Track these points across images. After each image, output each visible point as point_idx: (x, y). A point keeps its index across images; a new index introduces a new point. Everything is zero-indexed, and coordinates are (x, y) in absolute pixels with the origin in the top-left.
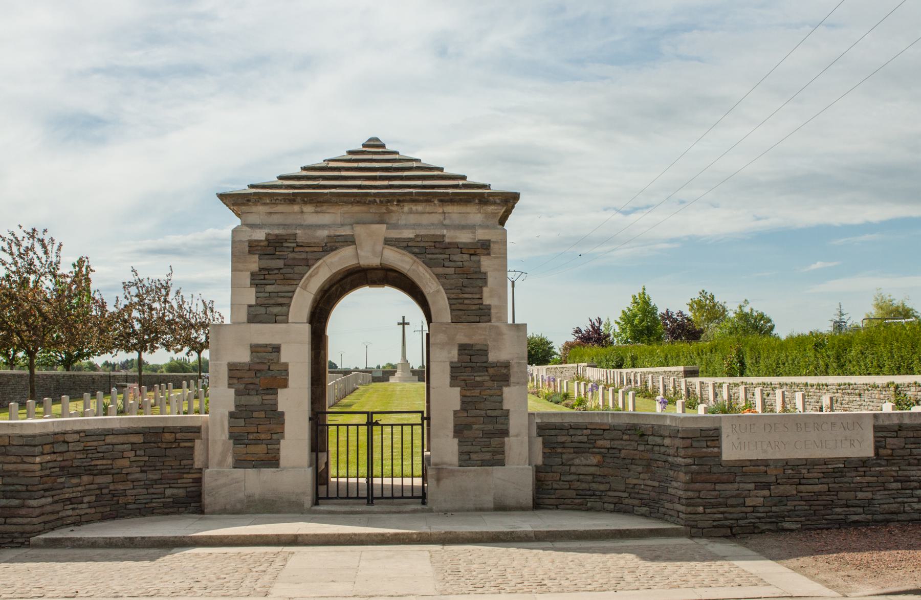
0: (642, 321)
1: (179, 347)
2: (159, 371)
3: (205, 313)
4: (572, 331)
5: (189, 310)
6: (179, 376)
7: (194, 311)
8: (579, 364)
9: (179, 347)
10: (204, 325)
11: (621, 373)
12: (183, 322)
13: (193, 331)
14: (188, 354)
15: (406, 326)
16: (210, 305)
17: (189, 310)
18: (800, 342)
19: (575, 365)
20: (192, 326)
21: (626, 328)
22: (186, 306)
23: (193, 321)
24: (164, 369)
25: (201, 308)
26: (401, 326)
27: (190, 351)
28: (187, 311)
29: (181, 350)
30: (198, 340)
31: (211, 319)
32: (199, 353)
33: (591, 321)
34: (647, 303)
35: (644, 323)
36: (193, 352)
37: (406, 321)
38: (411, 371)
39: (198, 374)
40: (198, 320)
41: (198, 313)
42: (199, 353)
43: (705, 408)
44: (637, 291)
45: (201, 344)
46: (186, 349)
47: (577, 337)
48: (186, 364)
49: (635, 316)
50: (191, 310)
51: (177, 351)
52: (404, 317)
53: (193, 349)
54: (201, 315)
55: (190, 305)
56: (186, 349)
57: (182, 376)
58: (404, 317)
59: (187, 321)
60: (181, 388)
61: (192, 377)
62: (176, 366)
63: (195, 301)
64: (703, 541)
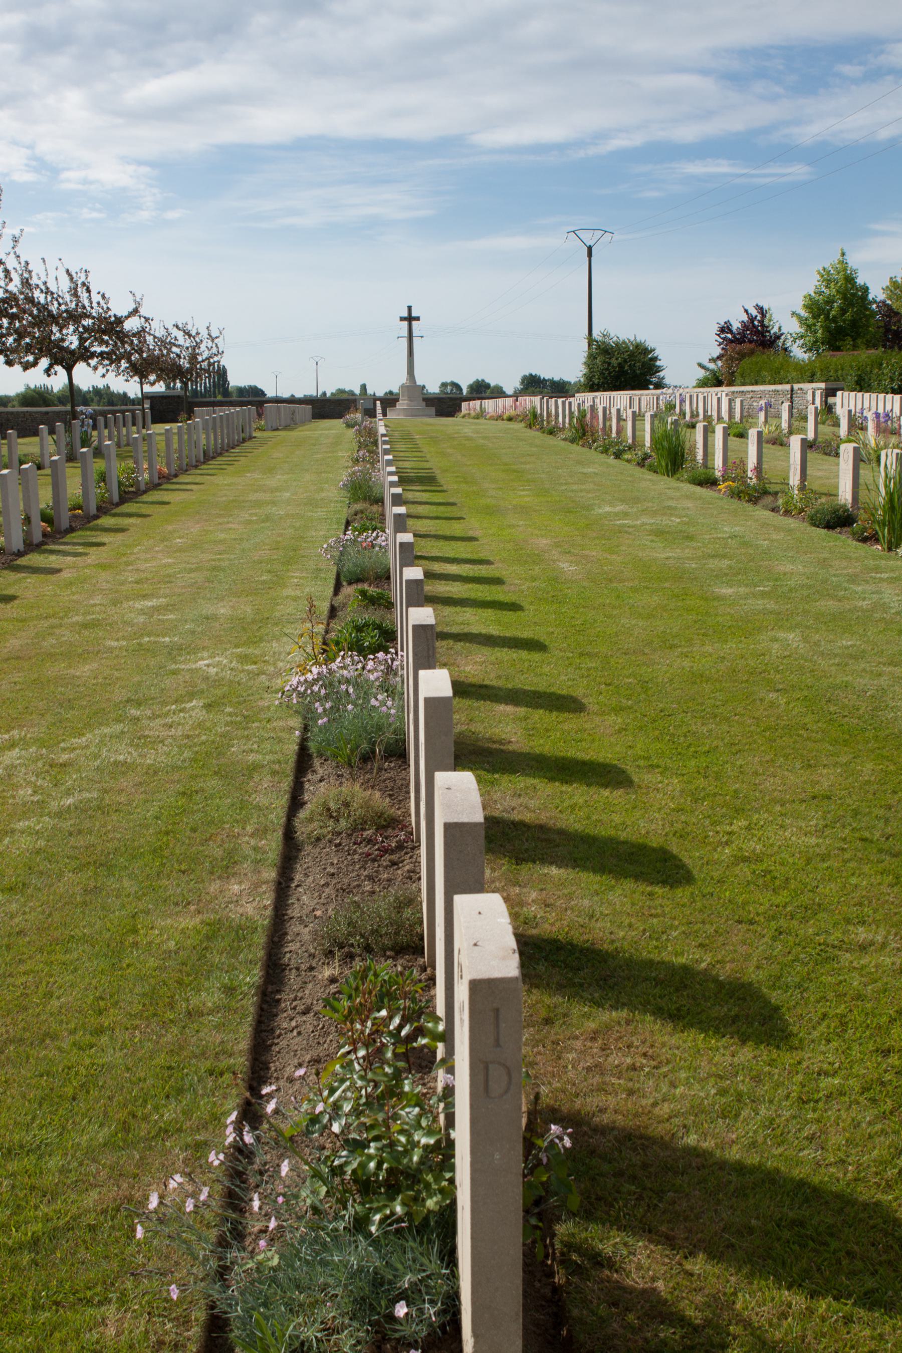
0: (843, 311)
1: (30, 358)
2: (10, 405)
3: (76, 295)
4: (715, 329)
5: (43, 288)
6: (36, 413)
7: (53, 288)
8: (796, 386)
9: (30, 358)
10: (74, 317)
11: (570, 403)
12: (35, 312)
13: (55, 329)
14: (48, 371)
15: (414, 323)
16: (83, 279)
17: (43, 288)
18: (241, 391)
19: (787, 387)
20: (54, 319)
21: (815, 325)
22: (34, 281)
23: (54, 308)
24: (15, 403)
25: (65, 285)
26: (406, 323)
27: (51, 366)
28: (42, 291)
29: (35, 364)
30: (66, 344)
31: (86, 303)
32: (69, 370)
33: (746, 311)
34: (850, 280)
35: (848, 315)
36: (58, 368)
37: (414, 314)
38: (424, 399)
39: (68, 408)
40: (63, 308)
41: (60, 293)
42: (69, 370)
43: (855, 448)
44: (830, 260)
45: (72, 352)
46: (44, 362)
47: (724, 339)
48: (48, 393)
49: (830, 302)
50: (47, 288)
51: (27, 367)
52: (410, 308)
53: (55, 361)
54: (68, 297)
55: (44, 279)
56: (44, 362)
57: (41, 413)
58: (410, 308)
59: (44, 308)
60: (38, 435)
61: (59, 416)
62: (32, 398)
63: (52, 274)
64: (442, 564)
